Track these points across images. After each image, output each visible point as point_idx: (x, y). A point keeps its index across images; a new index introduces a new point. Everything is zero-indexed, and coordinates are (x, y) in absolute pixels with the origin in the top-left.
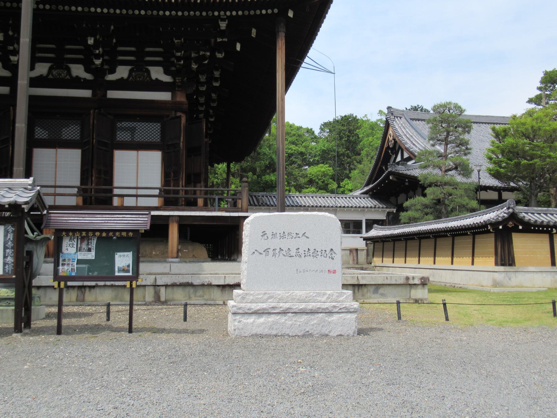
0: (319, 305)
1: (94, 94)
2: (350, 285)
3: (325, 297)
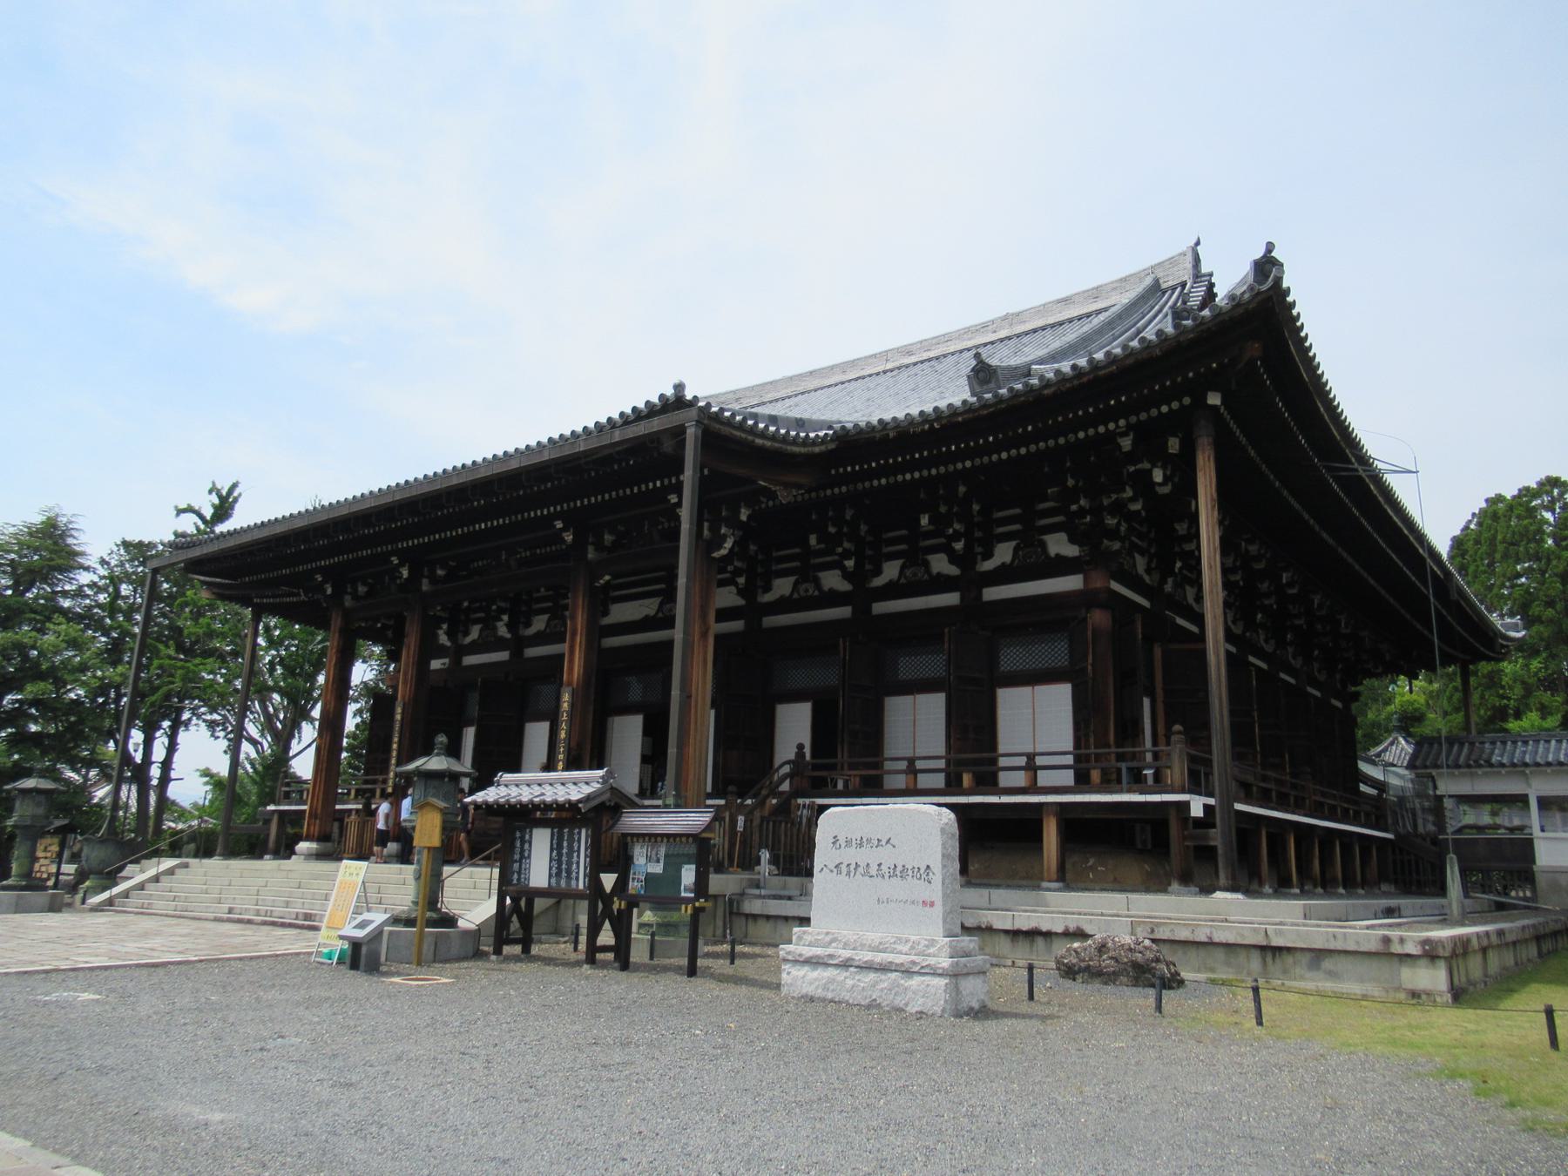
1: (962, 598)
2: (794, 918)
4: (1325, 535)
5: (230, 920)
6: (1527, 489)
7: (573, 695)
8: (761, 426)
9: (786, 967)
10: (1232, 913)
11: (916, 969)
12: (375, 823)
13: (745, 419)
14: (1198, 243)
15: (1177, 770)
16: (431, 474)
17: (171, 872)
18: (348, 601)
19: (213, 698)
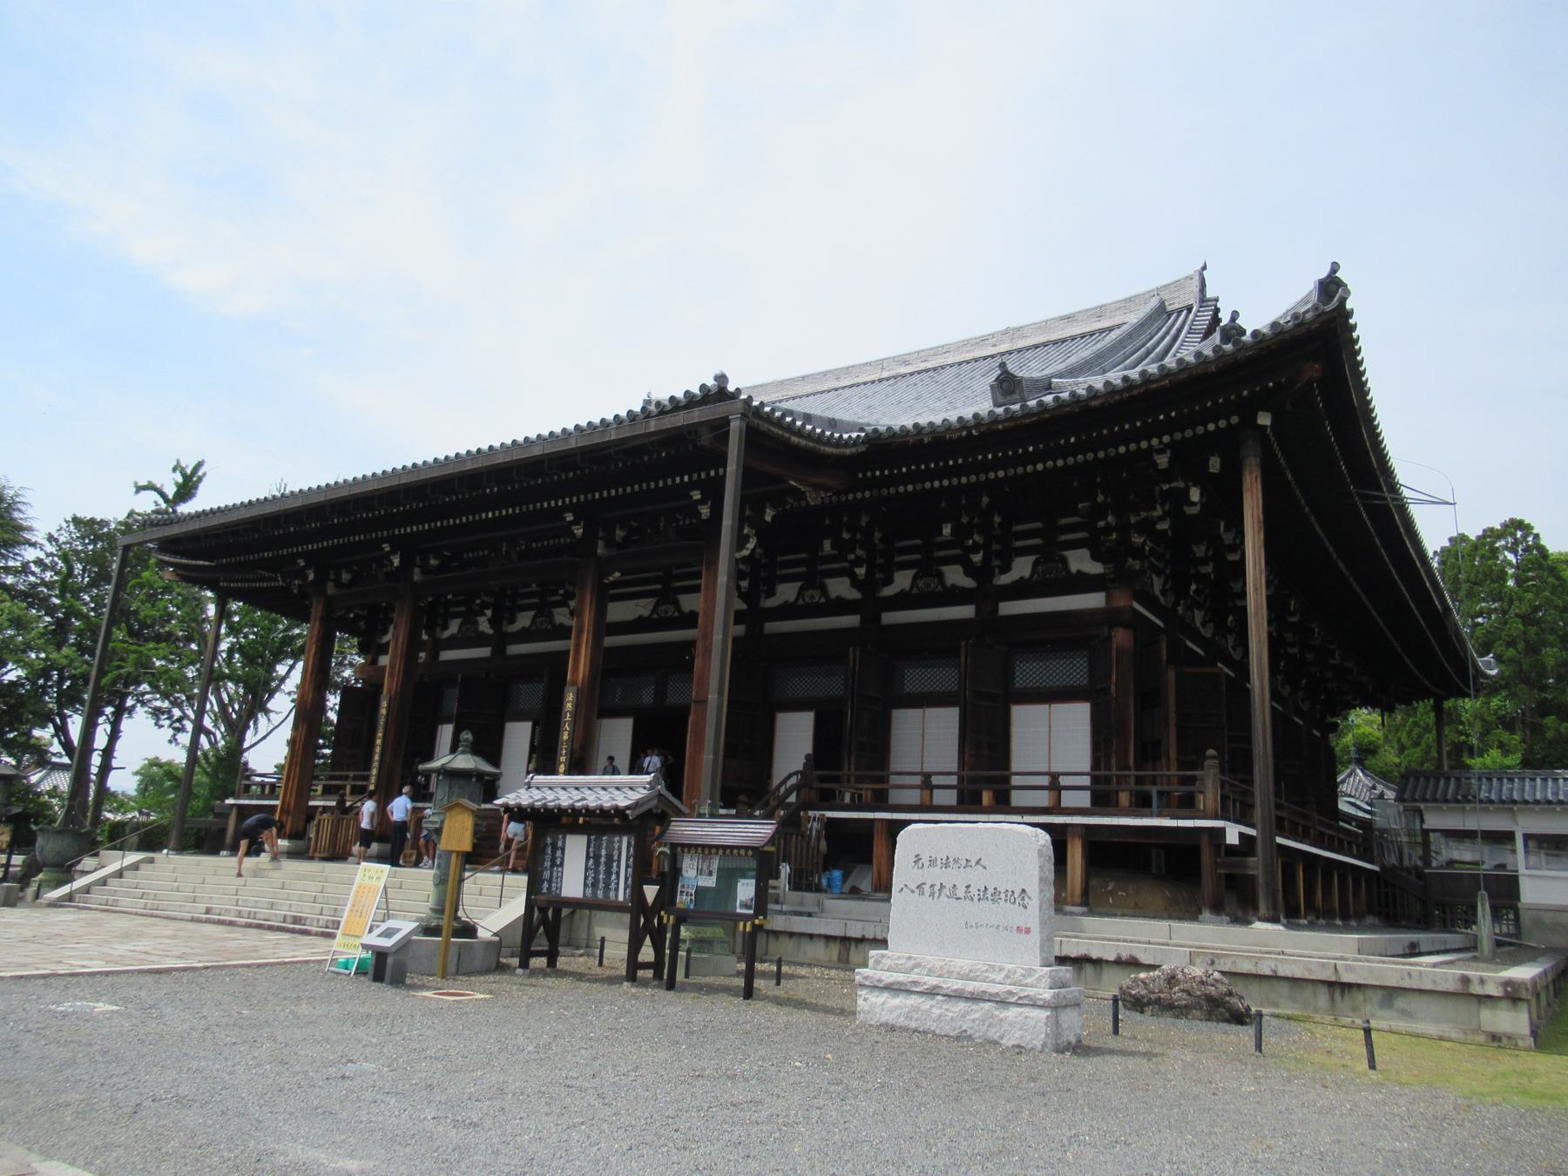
0: (984, 986)
1: (978, 612)
2: (820, 936)
3: (1003, 974)
4: (1341, 564)
5: (208, 921)
6: (1492, 530)
7: (578, 694)
8: (799, 423)
9: (863, 993)
10: (1269, 944)
11: (1013, 1000)
12: (358, 822)
13: (784, 416)
14: (1204, 268)
15: (1209, 795)
16: (442, 457)
17: (135, 867)
18: (331, 589)
19: (169, 685)
